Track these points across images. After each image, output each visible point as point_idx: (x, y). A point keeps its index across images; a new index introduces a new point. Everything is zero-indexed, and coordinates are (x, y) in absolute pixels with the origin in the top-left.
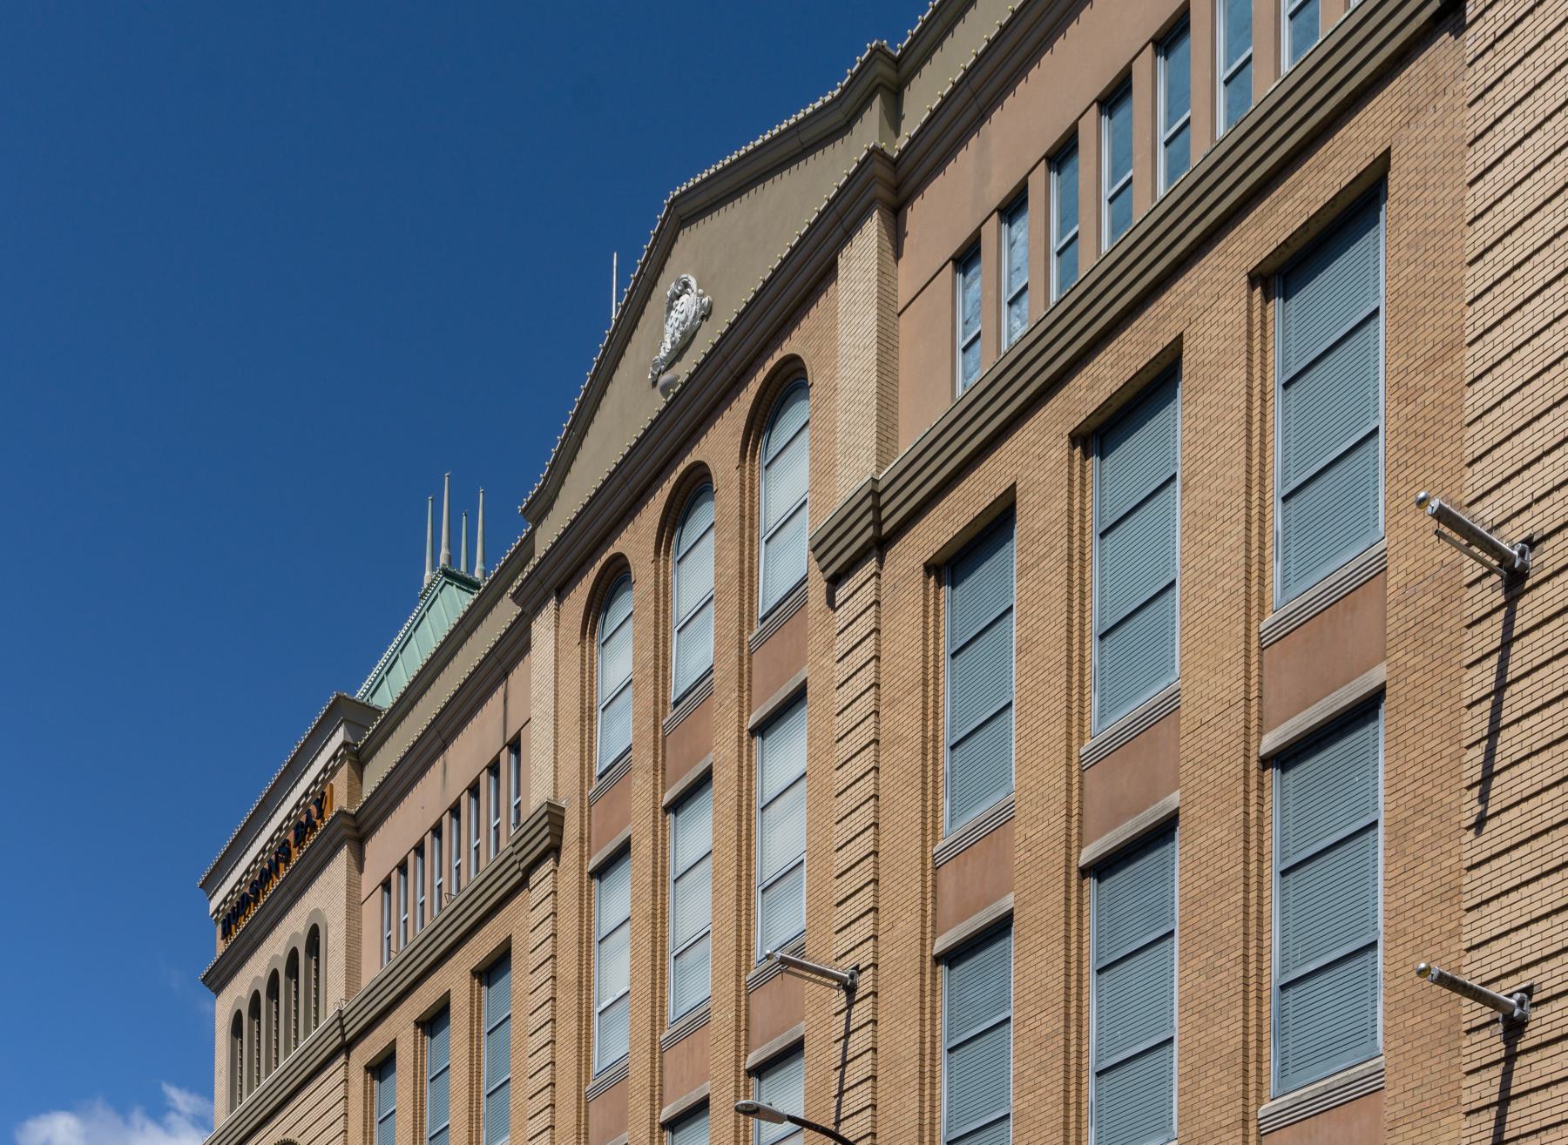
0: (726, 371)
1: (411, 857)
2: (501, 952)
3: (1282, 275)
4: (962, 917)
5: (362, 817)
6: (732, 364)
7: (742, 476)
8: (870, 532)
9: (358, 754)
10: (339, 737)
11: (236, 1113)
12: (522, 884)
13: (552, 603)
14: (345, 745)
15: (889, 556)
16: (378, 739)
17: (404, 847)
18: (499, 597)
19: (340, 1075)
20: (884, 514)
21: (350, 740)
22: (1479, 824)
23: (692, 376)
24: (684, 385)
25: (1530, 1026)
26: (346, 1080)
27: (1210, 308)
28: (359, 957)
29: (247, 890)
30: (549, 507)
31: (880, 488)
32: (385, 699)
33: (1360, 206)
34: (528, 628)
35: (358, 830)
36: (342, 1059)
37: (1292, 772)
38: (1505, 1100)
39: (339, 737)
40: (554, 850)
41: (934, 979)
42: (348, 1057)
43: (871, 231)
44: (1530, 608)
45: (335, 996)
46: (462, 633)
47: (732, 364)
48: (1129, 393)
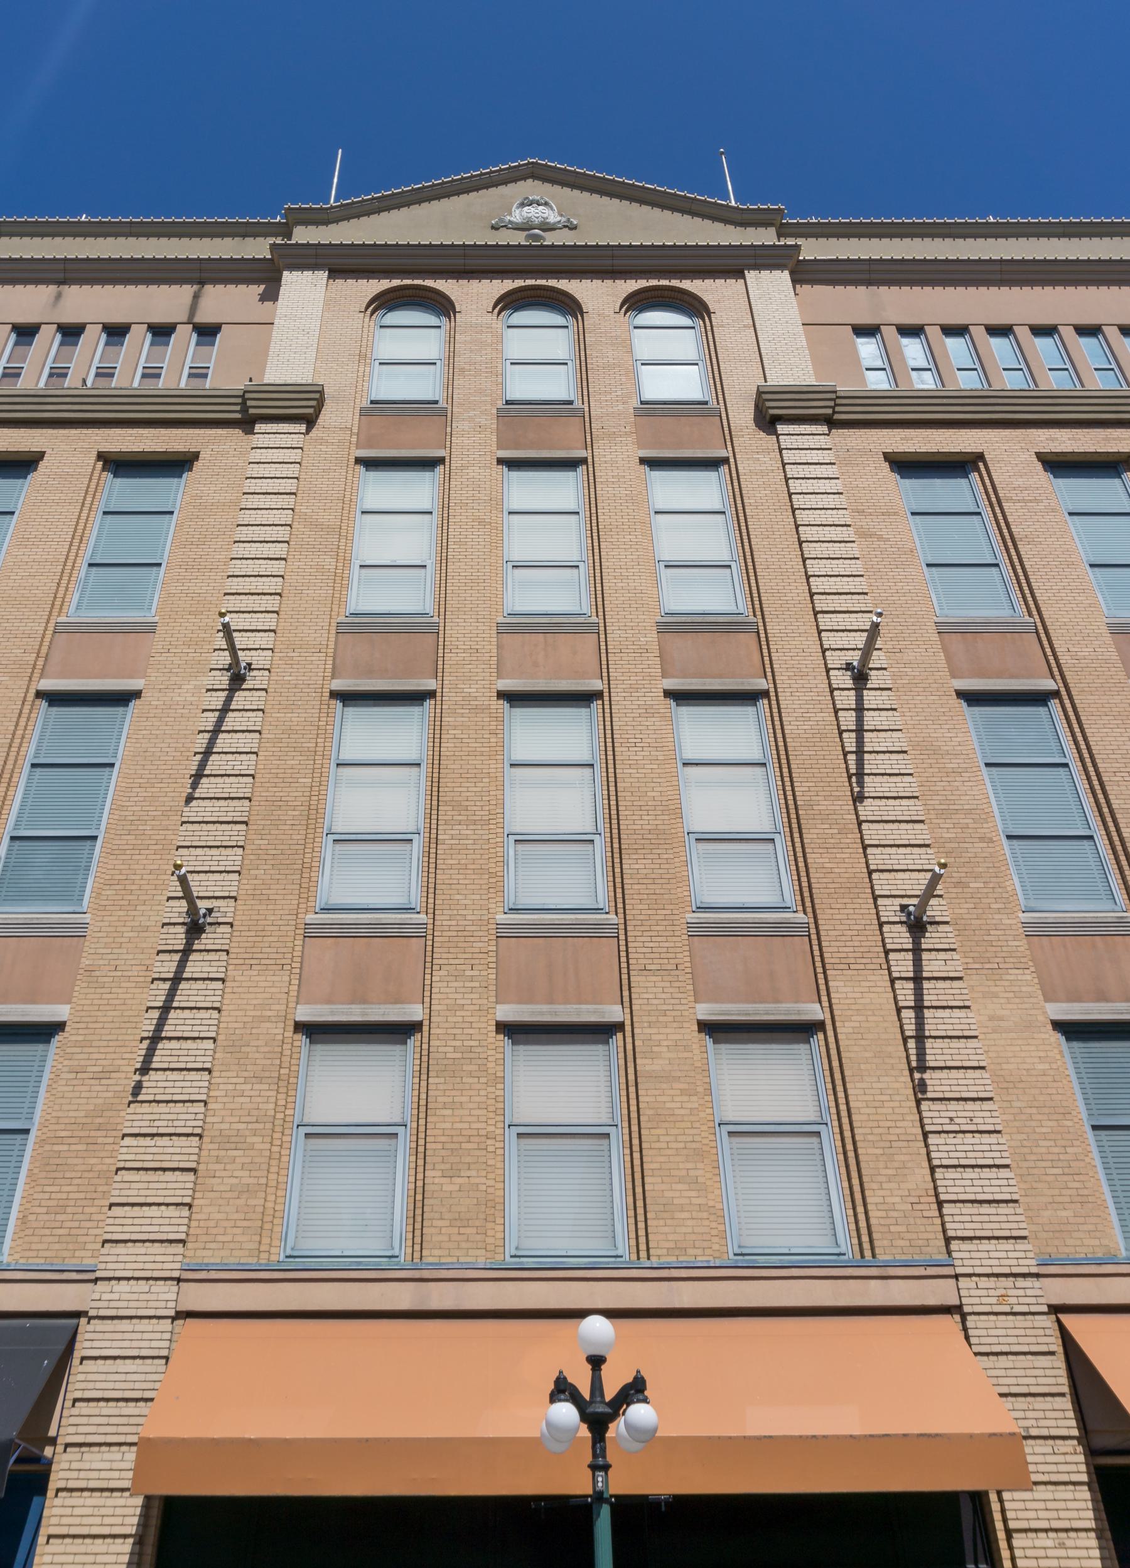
0: (609, 262)
3: (119, 465)
4: (62, 675)
18: (265, 235)
22: (190, 799)
23: (553, 246)
24: (542, 246)
25: (204, 936)
27: (69, 454)
30: (326, 223)
33: (177, 464)
37: (55, 709)
38: (177, 980)
44: (240, 699)
46: (127, 230)
48: (1081, 458)
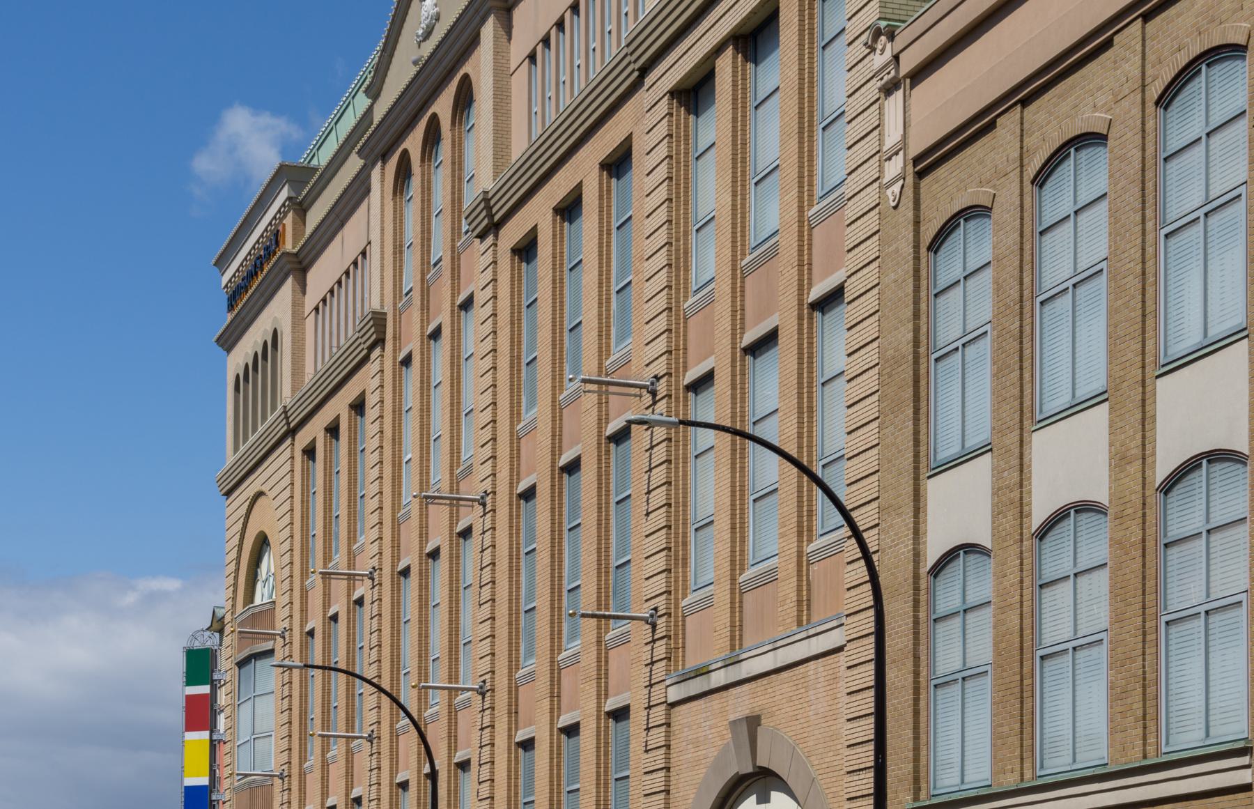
1: (568, 15)
2: (570, 199)
5: (301, 256)
6: (444, 64)
7: (453, 136)
8: (486, 221)
9: (300, 203)
10: (284, 194)
11: (239, 454)
12: (365, 359)
13: (379, 164)
14: (289, 198)
15: (502, 232)
16: (314, 193)
17: (330, 282)
19: (288, 454)
20: (494, 210)
21: (293, 195)
24: (427, 62)
26: (495, 262)
27: (646, 119)
28: (509, 132)
29: (262, 253)
31: (490, 195)
32: (323, 158)
34: (369, 176)
35: (301, 265)
36: (289, 441)
39: (284, 194)
40: (380, 341)
41: (743, 365)
42: (496, 236)
43: (379, 164)
45: (286, 395)
46: (348, 148)
47: (444, 64)
